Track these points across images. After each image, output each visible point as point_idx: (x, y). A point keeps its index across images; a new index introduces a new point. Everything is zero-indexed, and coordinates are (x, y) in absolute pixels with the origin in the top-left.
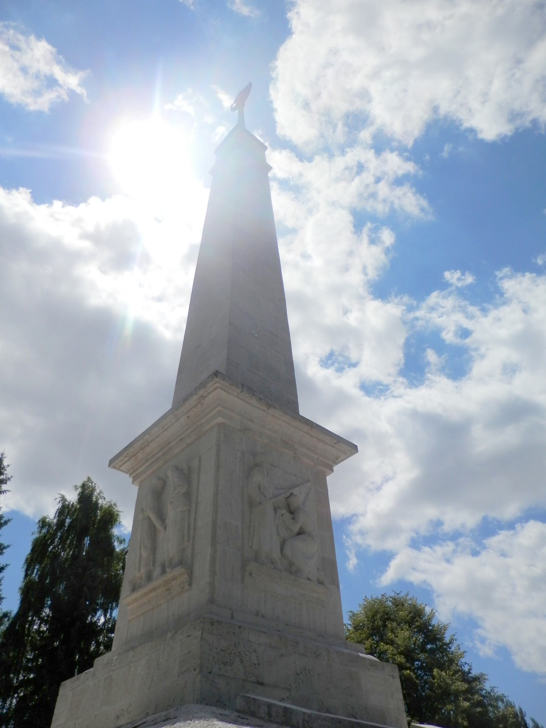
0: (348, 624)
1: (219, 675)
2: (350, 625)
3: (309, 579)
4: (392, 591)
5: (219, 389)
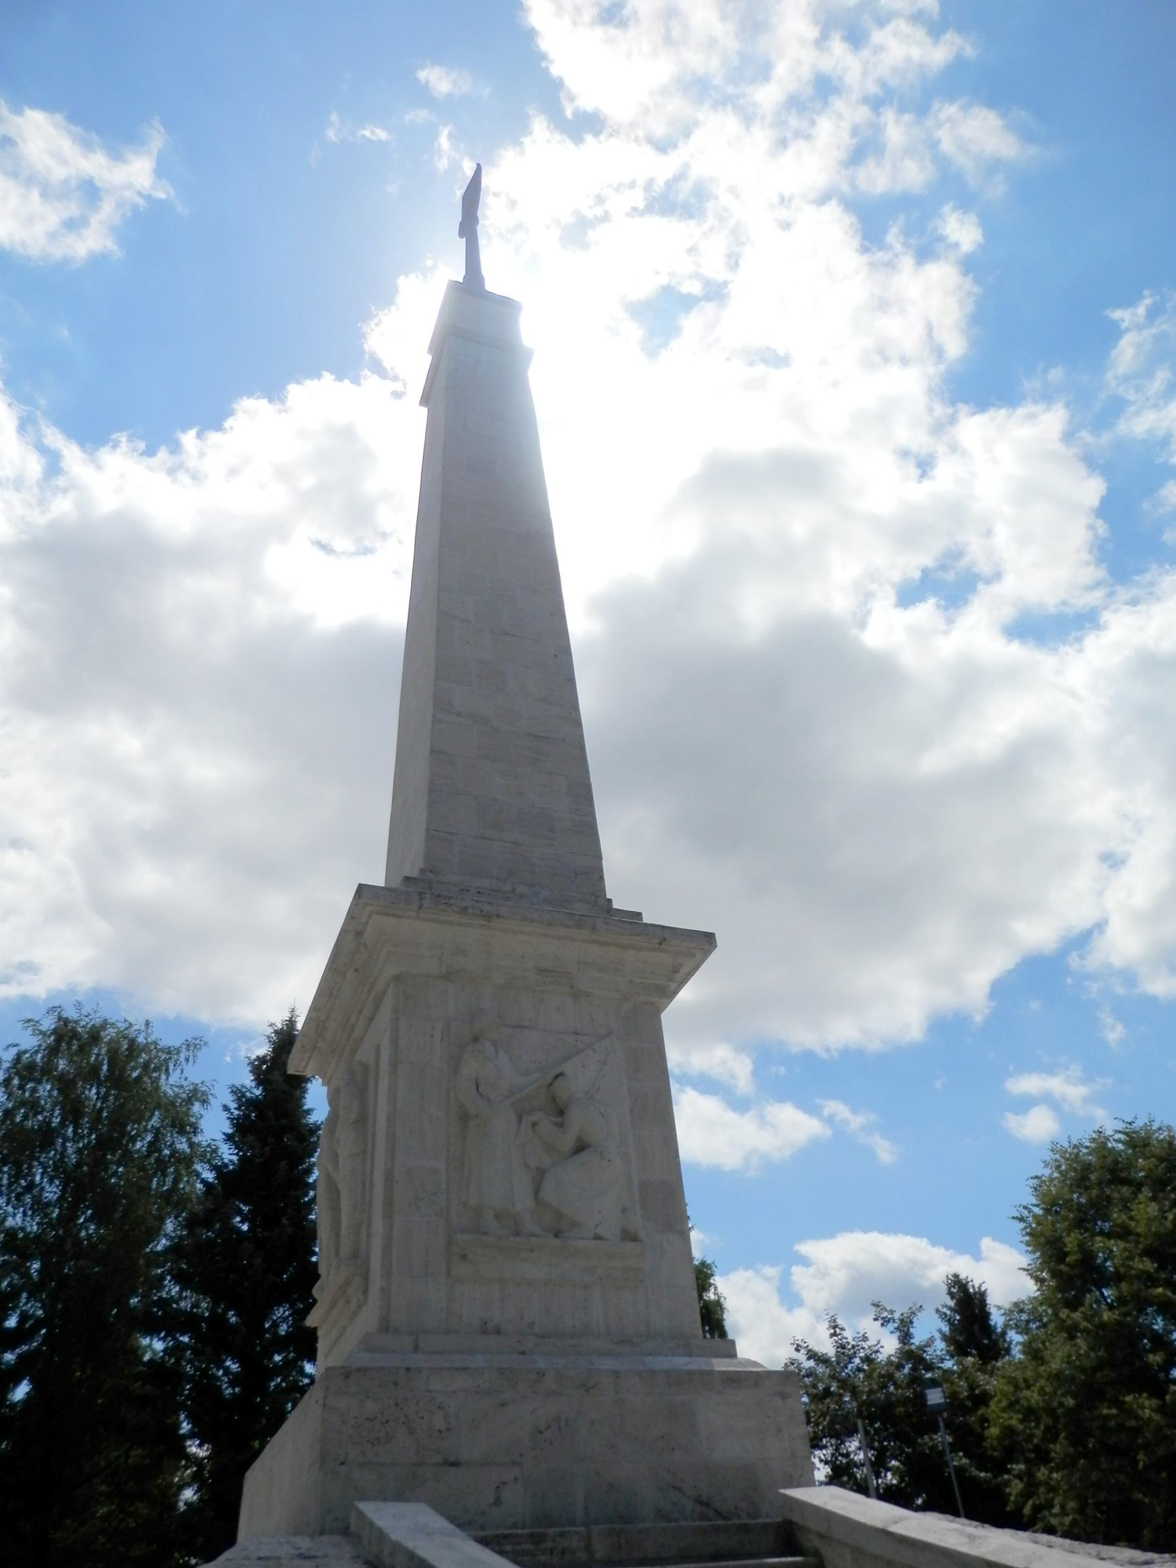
0: (1032, 1205)
1: (362, 1465)
2: (1037, 1206)
3: (598, 1237)
4: (1115, 1119)
5: (374, 915)
